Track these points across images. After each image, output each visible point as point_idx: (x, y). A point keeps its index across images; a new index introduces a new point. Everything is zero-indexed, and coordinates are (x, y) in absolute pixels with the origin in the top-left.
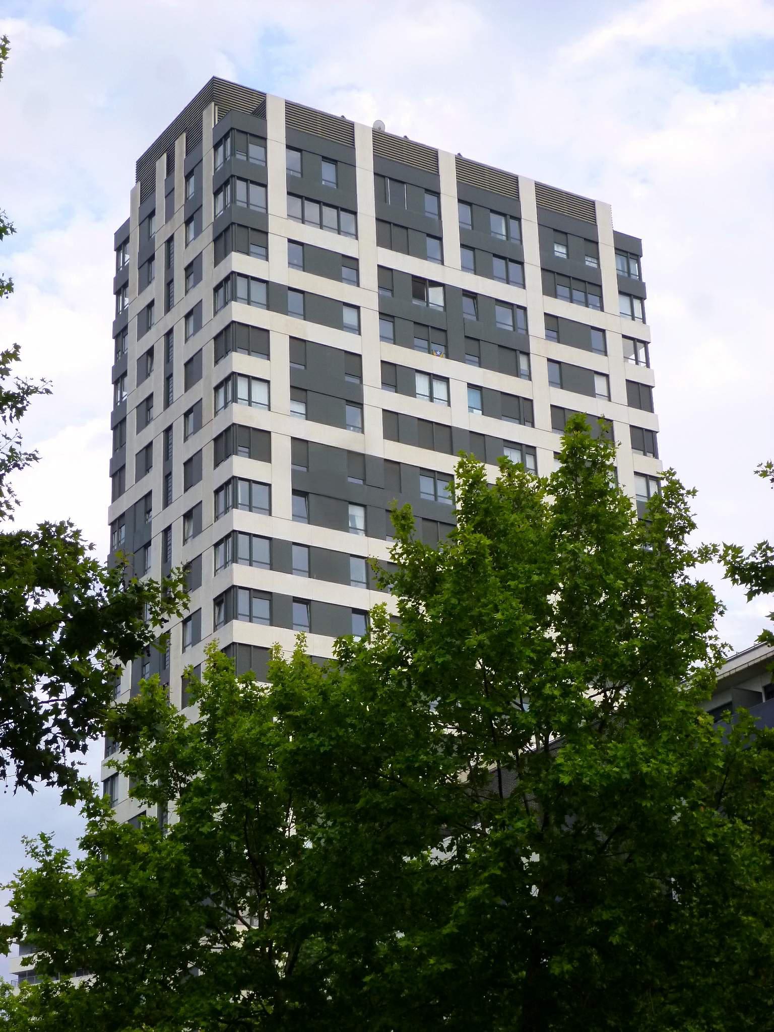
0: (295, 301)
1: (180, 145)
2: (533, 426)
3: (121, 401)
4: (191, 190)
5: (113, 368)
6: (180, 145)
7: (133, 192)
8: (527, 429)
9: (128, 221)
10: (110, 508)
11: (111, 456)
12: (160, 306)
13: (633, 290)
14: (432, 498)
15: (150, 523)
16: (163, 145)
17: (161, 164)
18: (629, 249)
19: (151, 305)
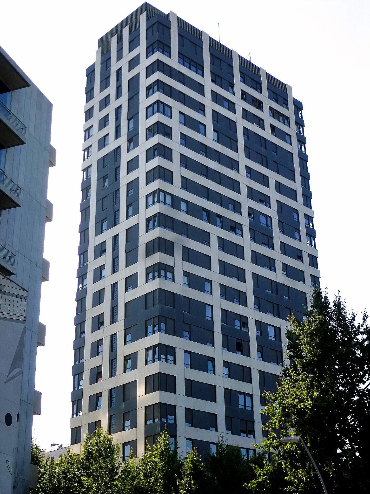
0: (183, 206)
1: (126, 31)
2: (273, 249)
3: (87, 178)
4: (131, 126)
5: (80, 226)
6: (126, 31)
7: (97, 52)
8: (270, 250)
9: (94, 64)
10: (85, 106)
11: (86, 86)
12: (107, 319)
13: (311, 234)
14: (243, 407)
15: (110, 69)
16: (117, 31)
17: (114, 40)
18: (298, 106)
19: (102, 267)
